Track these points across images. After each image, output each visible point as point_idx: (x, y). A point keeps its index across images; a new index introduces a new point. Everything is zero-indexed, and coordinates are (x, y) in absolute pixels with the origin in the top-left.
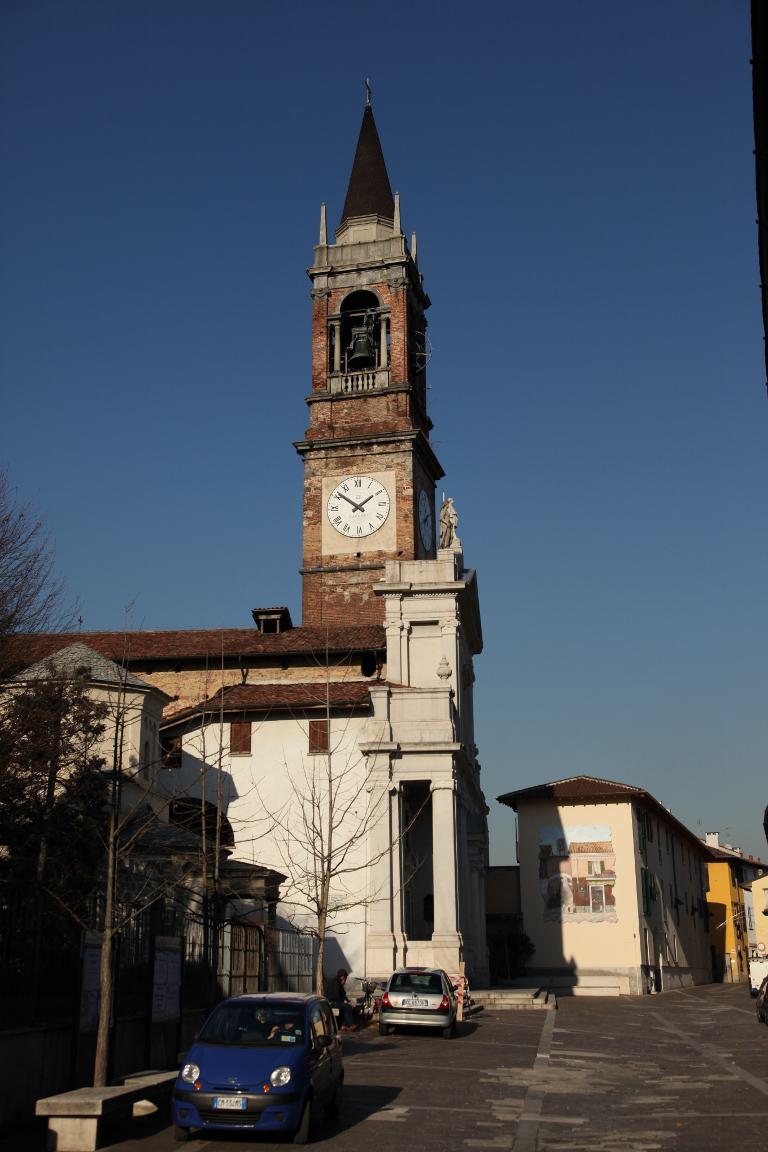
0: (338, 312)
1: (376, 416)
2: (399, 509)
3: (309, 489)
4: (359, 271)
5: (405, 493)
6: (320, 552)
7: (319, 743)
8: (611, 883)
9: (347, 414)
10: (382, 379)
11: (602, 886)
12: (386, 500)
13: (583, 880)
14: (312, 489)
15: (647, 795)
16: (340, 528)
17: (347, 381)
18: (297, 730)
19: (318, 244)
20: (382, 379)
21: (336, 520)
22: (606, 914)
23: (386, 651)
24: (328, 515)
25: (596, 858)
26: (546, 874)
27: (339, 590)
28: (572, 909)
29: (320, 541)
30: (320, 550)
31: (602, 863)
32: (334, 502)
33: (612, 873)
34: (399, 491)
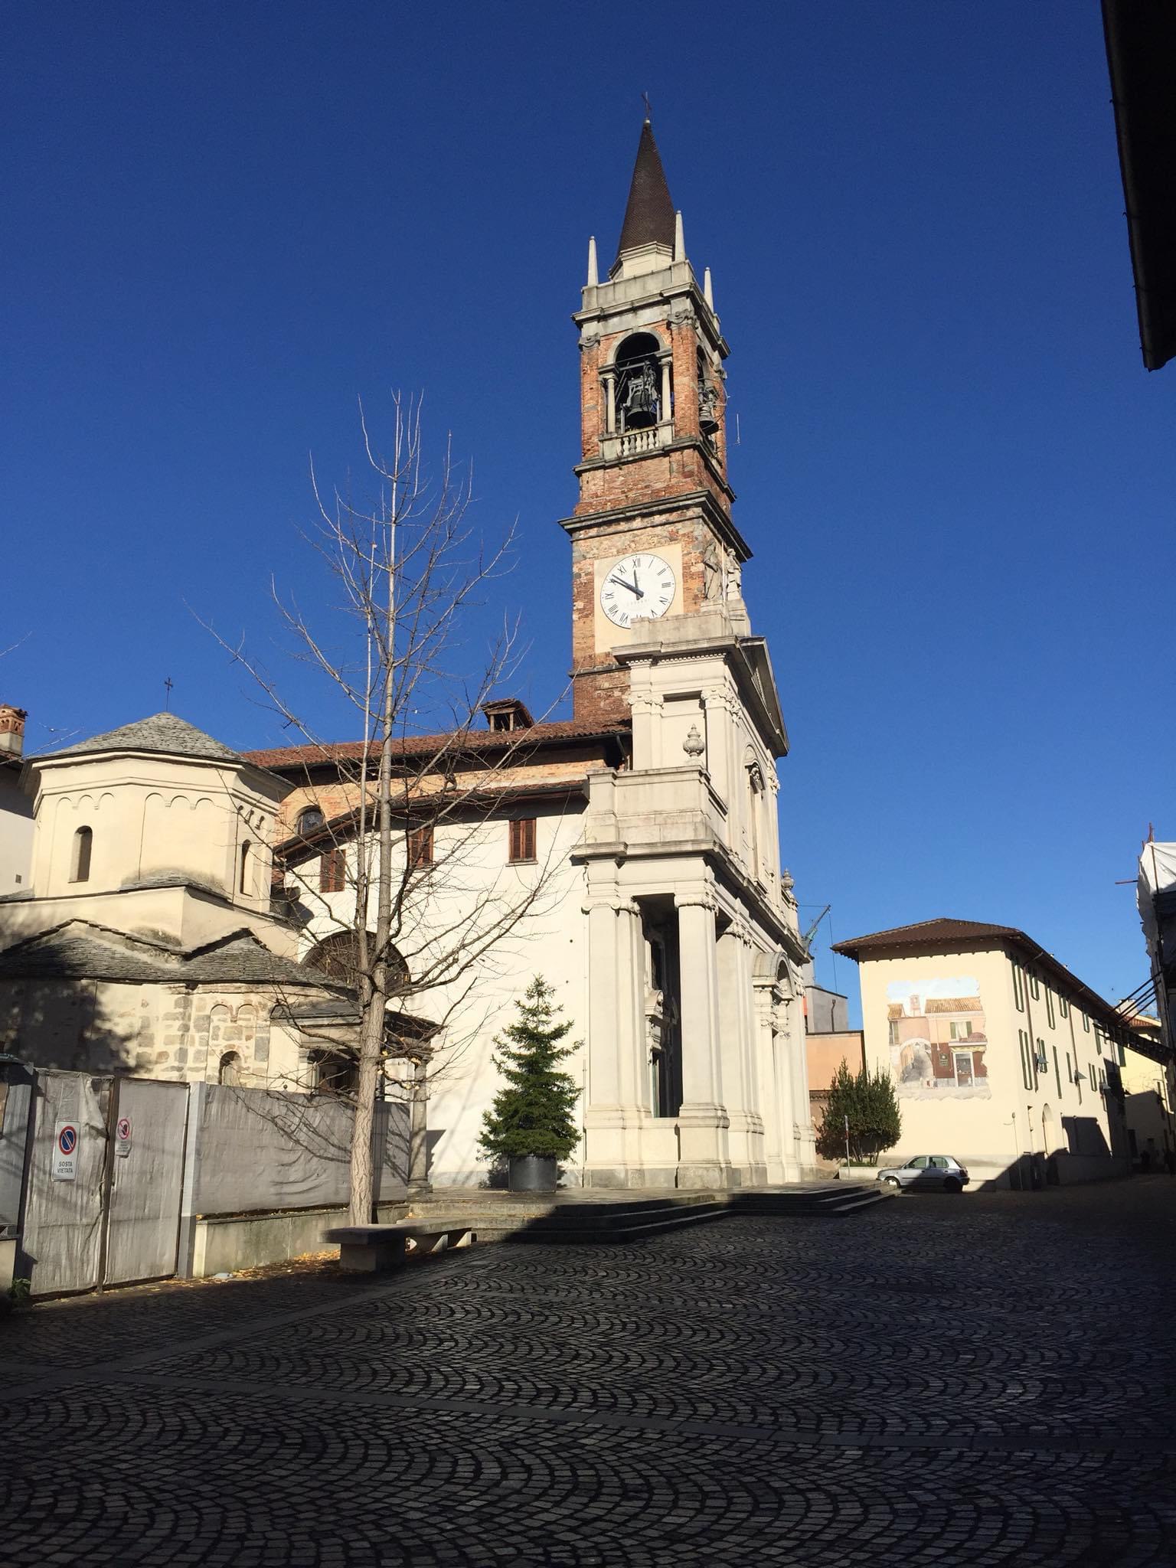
0: (611, 360)
1: (658, 481)
2: (687, 590)
3: (579, 576)
4: (634, 310)
5: (694, 569)
6: (593, 649)
7: (523, 851)
8: (981, 1049)
9: (624, 483)
10: (665, 436)
11: (969, 1053)
12: (670, 580)
13: (945, 1047)
14: (583, 575)
15: (1022, 935)
16: (616, 618)
17: (623, 443)
18: (497, 833)
19: (586, 285)
20: (665, 436)
21: (611, 610)
22: (975, 1089)
23: (631, 736)
24: (601, 603)
25: (960, 1018)
26: (897, 1038)
27: (617, 693)
28: (932, 1083)
29: (593, 636)
30: (592, 647)
31: (969, 1024)
32: (611, 587)
33: (981, 1037)
34: (686, 567)
